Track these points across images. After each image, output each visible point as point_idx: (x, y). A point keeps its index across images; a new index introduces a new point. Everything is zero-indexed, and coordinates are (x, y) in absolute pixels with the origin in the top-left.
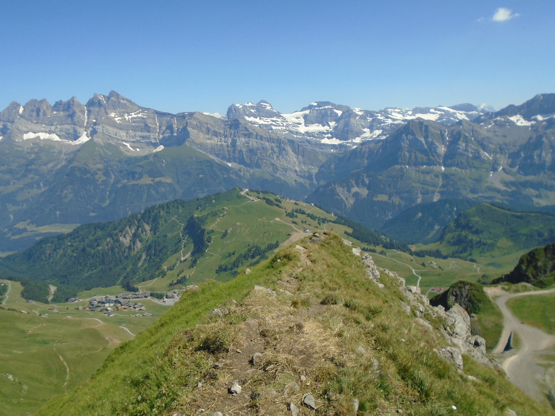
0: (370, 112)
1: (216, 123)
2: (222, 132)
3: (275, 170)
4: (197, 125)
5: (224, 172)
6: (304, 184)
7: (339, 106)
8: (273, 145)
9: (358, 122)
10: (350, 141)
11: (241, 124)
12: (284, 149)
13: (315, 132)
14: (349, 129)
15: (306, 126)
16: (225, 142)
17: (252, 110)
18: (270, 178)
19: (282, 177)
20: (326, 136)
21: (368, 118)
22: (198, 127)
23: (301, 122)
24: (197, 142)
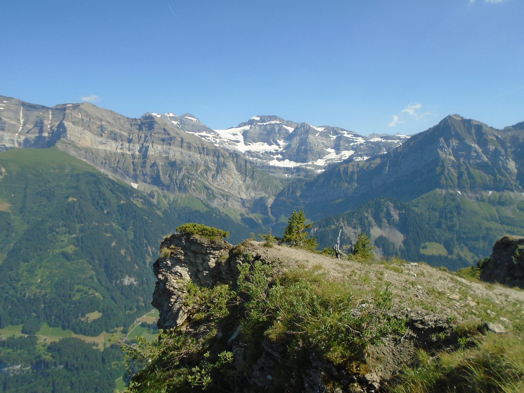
0: (333, 128)
1: (117, 120)
2: (126, 134)
3: (211, 196)
4: (82, 119)
5: (120, 195)
6: (255, 220)
7: (288, 121)
8: (207, 157)
9: (319, 140)
10: (310, 163)
11: (157, 123)
12: (225, 165)
13: (259, 152)
14: (308, 148)
15: (246, 144)
16: (129, 150)
17: (173, 122)
18: (203, 209)
19: (221, 208)
20: (275, 157)
21: (331, 136)
22: (85, 125)
23: (239, 140)
24: (79, 146)
